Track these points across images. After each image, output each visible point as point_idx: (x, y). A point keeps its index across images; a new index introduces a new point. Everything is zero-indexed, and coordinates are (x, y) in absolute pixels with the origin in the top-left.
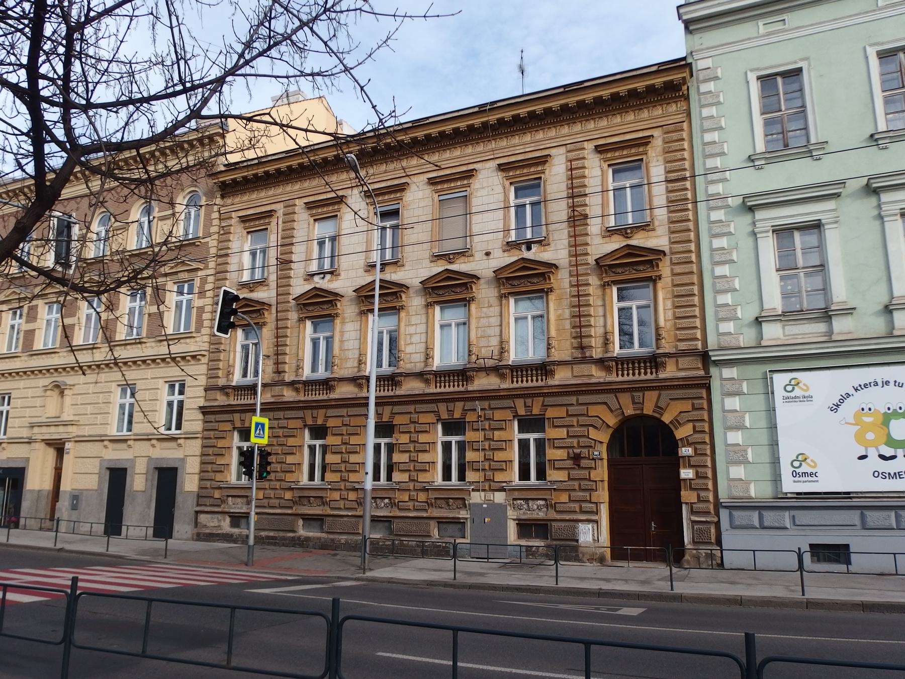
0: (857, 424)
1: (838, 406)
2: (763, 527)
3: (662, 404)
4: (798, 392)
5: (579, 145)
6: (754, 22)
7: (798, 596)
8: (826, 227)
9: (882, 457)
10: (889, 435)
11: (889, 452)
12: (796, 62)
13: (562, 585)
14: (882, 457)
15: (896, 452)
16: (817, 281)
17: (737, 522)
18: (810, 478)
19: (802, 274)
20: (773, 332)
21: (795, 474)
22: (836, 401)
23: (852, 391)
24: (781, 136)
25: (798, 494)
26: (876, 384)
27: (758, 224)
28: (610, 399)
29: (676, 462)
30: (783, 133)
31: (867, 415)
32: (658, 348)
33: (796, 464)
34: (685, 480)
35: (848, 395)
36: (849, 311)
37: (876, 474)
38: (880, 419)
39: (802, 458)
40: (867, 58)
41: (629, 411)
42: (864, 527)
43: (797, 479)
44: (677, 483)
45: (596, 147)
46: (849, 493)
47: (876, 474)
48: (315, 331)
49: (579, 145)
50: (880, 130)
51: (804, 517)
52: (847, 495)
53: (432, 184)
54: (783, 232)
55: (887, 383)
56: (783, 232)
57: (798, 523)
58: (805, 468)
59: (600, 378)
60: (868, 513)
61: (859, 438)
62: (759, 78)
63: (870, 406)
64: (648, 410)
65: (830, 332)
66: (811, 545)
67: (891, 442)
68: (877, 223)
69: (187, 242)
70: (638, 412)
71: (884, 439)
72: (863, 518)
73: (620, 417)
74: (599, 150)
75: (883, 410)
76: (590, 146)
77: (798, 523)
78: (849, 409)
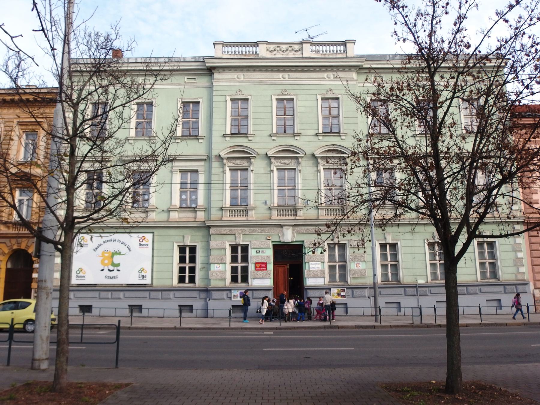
0: (102, 257)
1: (97, 249)
2: (150, 299)
3: (29, 245)
4: (144, 242)
5: (11, 120)
6: (183, 77)
7: (434, 322)
8: (200, 172)
9: (109, 270)
10: (113, 261)
11: (111, 268)
12: (197, 99)
13: (483, 322)
14: (109, 270)
15: (104, 267)
16: (292, 193)
17: (408, 294)
18: (82, 278)
19: (189, 192)
20: (174, 216)
21: (77, 276)
22: (96, 247)
23: (102, 243)
24: (283, 127)
25: (128, 285)
26: (111, 241)
27: (174, 168)
28: (7, 241)
29: (32, 270)
30: (284, 125)
31: (106, 253)
32: (31, 219)
33: (78, 272)
34: (34, 278)
35: (101, 245)
36: (254, 208)
37: (106, 277)
38: (111, 255)
39: (80, 270)
40: (272, 100)
41: (15, 247)
42: (353, 296)
43: (77, 278)
44: (31, 280)
45: (18, 122)
46: (146, 284)
47: (106, 277)
48: (21, 195)
49: (11, 120)
50: (227, 133)
51: (128, 294)
52: (95, 285)
53: (21, 125)
54: (183, 172)
55: (115, 240)
56: (183, 172)
57: (432, 292)
58: (81, 274)
59: (4, 231)
60: (407, 289)
61: (102, 262)
62: (276, 99)
63: (108, 249)
64: (23, 247)
65: (195, 218)
66: (179, 306)
67: (113, 265)
68: (171, 174)
69: (27, 131)
70: (19, 248)
71: (111, 263)
72: (353, 292)
73: (11, 250)
74: (20, 124)
75: (112, 251)
76: (16, 121)
77: (432, 292)
78: (100, 250)
